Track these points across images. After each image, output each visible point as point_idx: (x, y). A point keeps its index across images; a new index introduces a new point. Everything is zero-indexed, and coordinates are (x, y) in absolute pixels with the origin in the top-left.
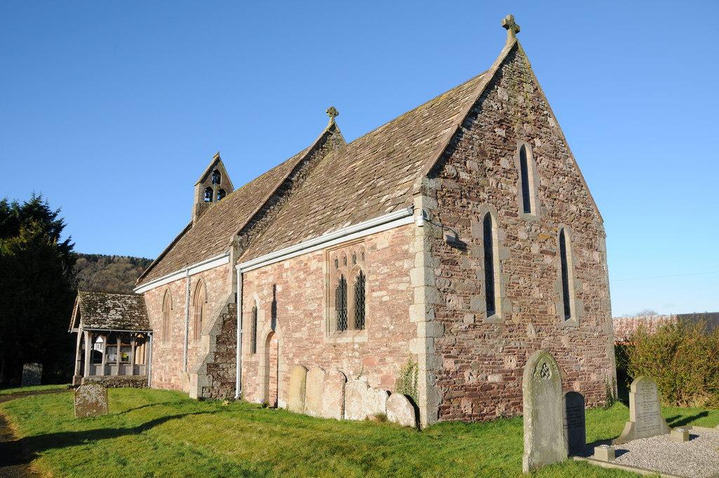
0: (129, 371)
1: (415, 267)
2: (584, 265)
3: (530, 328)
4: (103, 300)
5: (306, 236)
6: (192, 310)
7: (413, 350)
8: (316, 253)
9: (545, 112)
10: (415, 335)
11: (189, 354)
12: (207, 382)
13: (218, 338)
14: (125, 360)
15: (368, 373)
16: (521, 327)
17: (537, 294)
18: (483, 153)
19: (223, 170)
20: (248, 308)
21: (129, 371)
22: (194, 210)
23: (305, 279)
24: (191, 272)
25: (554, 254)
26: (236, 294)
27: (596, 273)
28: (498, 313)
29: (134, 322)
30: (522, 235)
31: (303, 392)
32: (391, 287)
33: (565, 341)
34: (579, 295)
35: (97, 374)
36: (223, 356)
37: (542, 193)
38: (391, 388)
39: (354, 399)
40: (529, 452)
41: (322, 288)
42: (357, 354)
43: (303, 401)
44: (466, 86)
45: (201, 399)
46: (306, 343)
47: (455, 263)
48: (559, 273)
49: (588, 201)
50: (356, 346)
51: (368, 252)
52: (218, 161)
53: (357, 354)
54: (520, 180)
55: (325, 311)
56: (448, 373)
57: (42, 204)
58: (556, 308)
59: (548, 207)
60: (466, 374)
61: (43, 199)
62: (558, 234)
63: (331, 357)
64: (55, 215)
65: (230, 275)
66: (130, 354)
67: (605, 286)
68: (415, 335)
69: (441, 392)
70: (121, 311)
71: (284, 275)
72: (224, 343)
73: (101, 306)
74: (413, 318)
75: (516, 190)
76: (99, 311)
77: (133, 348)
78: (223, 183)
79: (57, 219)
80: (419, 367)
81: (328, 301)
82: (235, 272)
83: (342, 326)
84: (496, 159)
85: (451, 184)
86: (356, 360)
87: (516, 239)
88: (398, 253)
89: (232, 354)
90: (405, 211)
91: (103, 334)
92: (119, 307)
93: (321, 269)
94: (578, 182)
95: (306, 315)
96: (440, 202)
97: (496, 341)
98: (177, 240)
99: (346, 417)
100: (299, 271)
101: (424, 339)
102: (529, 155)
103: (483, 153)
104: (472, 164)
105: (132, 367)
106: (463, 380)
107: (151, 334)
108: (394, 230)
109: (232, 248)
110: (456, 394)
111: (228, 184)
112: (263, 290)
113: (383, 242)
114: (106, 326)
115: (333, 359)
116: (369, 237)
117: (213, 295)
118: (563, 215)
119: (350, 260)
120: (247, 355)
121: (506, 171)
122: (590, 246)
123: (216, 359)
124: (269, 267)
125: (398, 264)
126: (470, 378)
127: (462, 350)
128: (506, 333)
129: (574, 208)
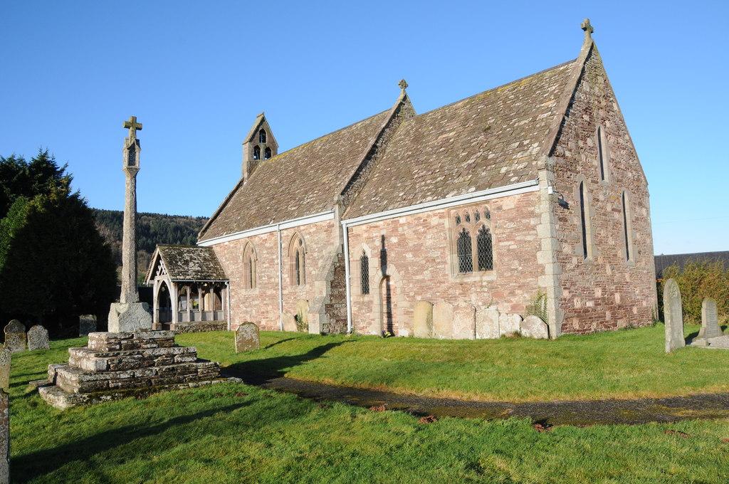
0: (198, 317)
1: (541, 223)
2: (637, 219)
3: (608, 268)
4: (181, 254)
5: (424, 197)
6: (287, 260)
7: (541, 284)
8: (437, 212)
9: (611, 99)
10: (543, 273)
11: (285, 298)
12: (326, 319)
13: (332, 283)
14: (195, 307)
15: (497, 303)
16: (603, 266)
17: (611, 242)
18: (577, 135)
19: (268, 128)
20: (356, 256)
21: (198, 317)
22: (245, 168)
23: (424, 232)
24: (281, 227)
25: (619, 211)
26: (343, 246)
27: (643, 223)
28: (590, 256)
29: (212, 273)
30: (601, 198)
31: (429, 322)
32: (518, 238)
33: (627, 276)
34: (635, 242)
35: (184, 320)
36: (336, 297)
37: (612, 164)
38: (523, 312)
39: (486, 323)
40: (669, 340)
41: (445, 239)
42: (486, 290)
43: (430, 328)
44: (548, 74)
45: (323, 334)
46: (429, 283)
47: (566, 220)
48: (623, 226)
49: (638, 169)
50: (484, 284)
51: (493, 212)
52: (263, 120)
53: (486, 290)
54: (598, 155)
55: (449, 257)
56: (565, 299)
57: (49, 159)
58: (621, 253)
59: (615, 175)
60: (575, 300)
61: (50, 155)
62: (621, 195)
63: (457, 293)
64: (62, 170)
65: (336, 231)
66: (199, 301)
67: (649, 235)
68: (543, 273)
69: (563, 314)
70: (198, 263)
71: (400, 229)
72: (336, 286)
73: (180, 260)
74: (540, 261)
75: (596, 163)
76: (179, 263)
77: (200, 295)
78: (269, 142)
79: (64, 174)
80: (548, 296)
81: (451, 250)
82: (341, 227)
83: (465, 267)
84: (584, 139)
85: (561, 161)
86: (485, 294)
87: (598, 200)
88: (524, 211)
89: (342, 297)
90: (533, 182)
91: (188, 284)
92: (195, 259)
93: (443, 224)
94: (632, 154)
95: (428, 261)
96: (556, 175)
97: (590, 277)
98: (231, 195)
99: (478, 337)
100: (417, 225)
101: (552, 276)
102: (602, 135)
103: (577, 135)
104: (571, 144)
105: (201, 313)
106: (573, 305)
107: (228, 283)
108: (519, 196)
109: (337, 206)
110: (571, 315)
111: (273, 142)
112: (374, 241)
113: (509, 204)
114: (190, 277)
115: (460, 294)
116: (493, 200)
117: (315, 246)
118: (624, 180)
119: (472, 218)
120: (358, 296)
121: (591, 149)
122: (640, 204)
123: (331, 300)
124: (381, 223)
125: (524, 221)
126: (578, 304)
127: (573, 284)
128: (595, 271)
129: (630, 175)
